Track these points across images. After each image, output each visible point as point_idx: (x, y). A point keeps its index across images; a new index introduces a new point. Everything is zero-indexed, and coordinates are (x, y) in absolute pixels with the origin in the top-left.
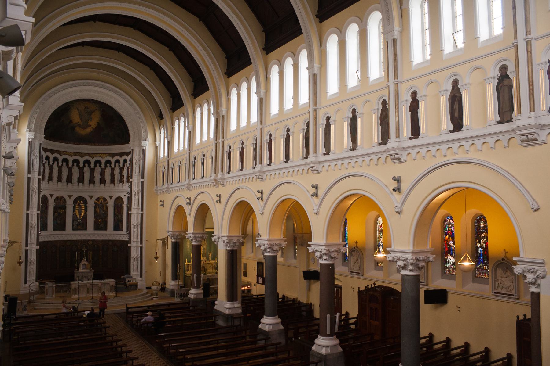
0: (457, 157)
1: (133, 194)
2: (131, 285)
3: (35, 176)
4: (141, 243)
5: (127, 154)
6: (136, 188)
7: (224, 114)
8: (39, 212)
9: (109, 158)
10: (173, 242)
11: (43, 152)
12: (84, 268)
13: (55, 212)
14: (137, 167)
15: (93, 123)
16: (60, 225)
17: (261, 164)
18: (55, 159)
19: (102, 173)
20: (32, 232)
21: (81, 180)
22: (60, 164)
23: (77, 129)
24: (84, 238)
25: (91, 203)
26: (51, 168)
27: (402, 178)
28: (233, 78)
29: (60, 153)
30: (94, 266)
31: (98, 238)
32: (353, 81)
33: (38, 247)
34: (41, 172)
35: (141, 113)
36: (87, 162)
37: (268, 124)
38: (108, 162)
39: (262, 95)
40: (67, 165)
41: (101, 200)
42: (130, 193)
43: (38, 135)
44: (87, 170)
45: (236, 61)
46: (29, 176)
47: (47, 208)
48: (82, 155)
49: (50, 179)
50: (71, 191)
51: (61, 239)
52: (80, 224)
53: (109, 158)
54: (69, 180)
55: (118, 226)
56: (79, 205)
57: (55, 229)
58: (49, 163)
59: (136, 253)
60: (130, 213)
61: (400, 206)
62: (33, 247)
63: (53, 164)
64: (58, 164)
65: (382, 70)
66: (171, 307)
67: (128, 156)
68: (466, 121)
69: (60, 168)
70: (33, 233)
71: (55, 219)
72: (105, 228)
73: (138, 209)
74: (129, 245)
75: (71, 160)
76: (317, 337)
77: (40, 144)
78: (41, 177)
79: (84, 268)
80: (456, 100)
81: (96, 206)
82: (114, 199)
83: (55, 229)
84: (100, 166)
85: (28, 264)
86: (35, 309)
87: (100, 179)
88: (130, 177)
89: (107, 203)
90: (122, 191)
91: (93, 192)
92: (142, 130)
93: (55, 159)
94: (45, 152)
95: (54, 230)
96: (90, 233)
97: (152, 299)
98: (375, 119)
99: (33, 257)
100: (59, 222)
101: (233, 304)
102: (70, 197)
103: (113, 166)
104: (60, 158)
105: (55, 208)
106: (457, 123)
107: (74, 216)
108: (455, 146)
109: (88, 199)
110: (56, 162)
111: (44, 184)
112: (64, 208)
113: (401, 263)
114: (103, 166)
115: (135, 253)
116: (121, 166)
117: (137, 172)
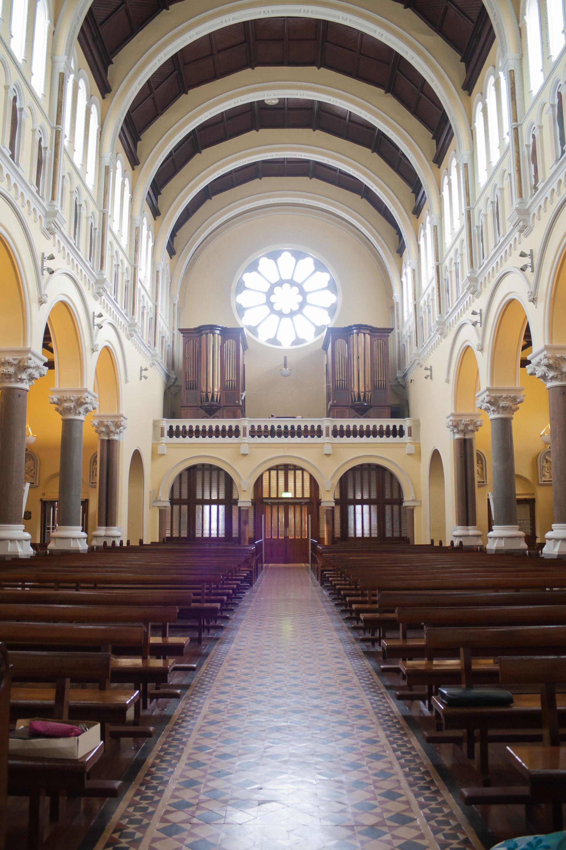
7: (398, 301)
17: (417, 346)
101: (468, 530)
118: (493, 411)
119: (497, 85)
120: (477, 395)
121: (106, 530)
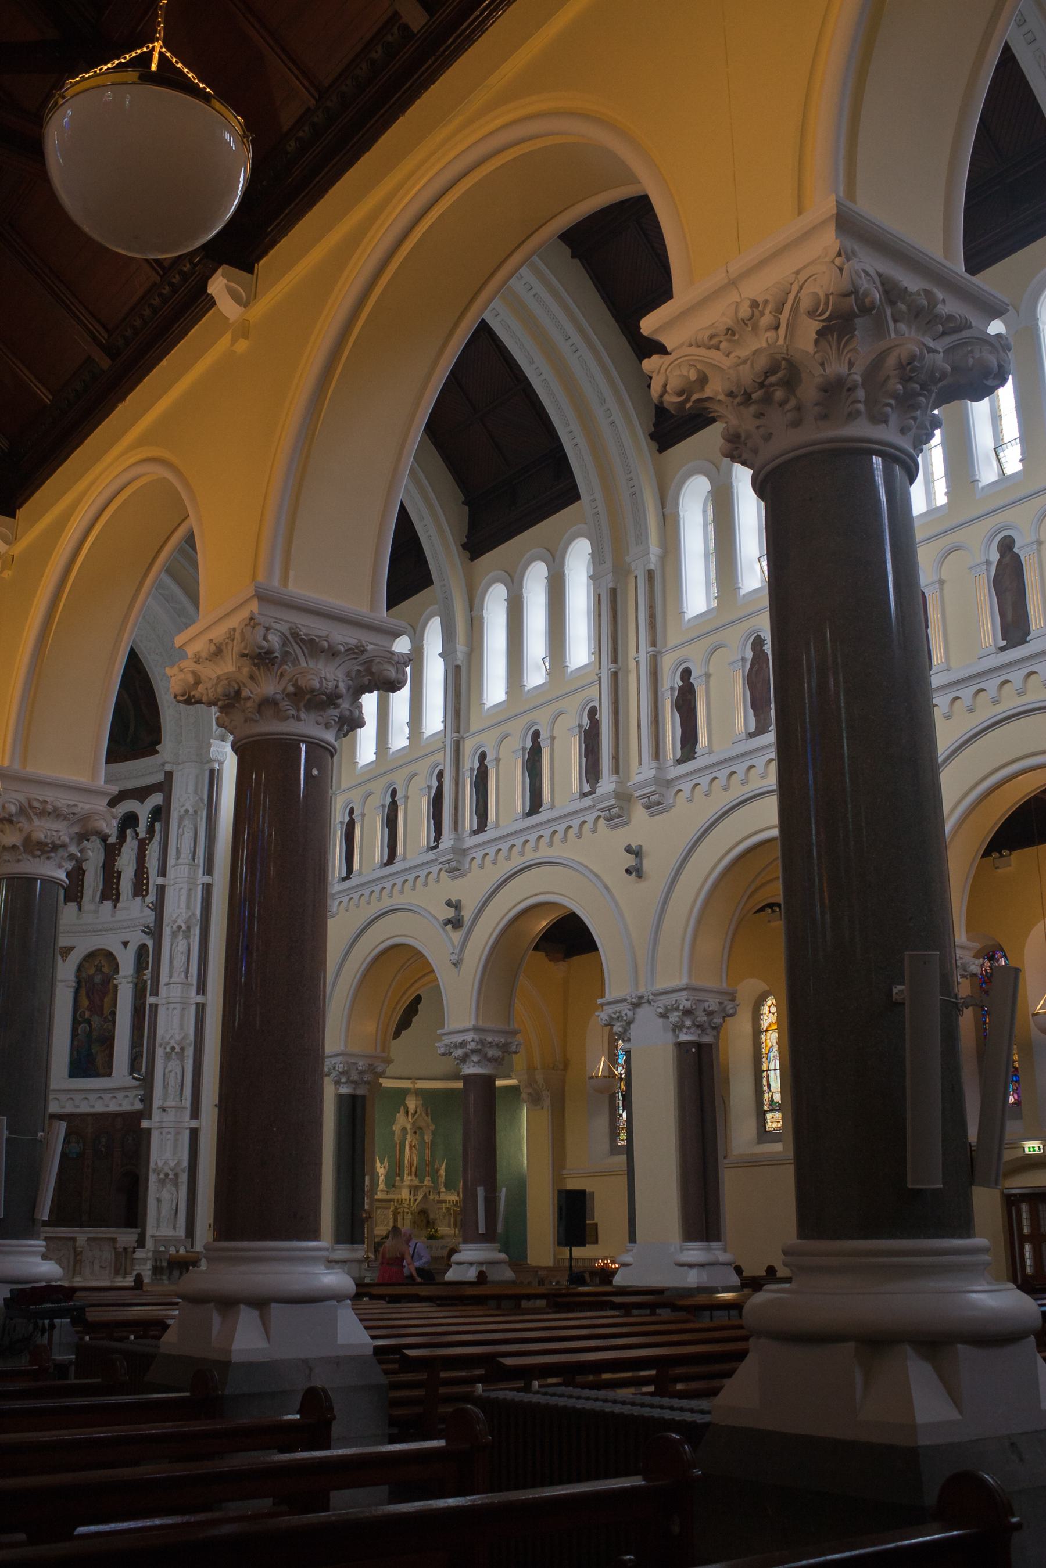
0: (1024, 700)
1: (167, 932)
10: (340, 1097)
14: (188, 836)
27: (644, 848)
28: (486, 559)
32: (535, 676)
37: (473, 728)
39: (460, 657)
42: (155, 931)
61: (457, 951)
65: (713, 597)
68: (1036, 619)
73: (186, 985)
74: (145, 1124)
98: (424, 807)
103: (142, 830)
108: (1017, 676)
113: (459, 1052)
115: (168, 1155)
116: (142, 835)
118: (479, 1062)
119: (722, 506)
120: (439, 1032)
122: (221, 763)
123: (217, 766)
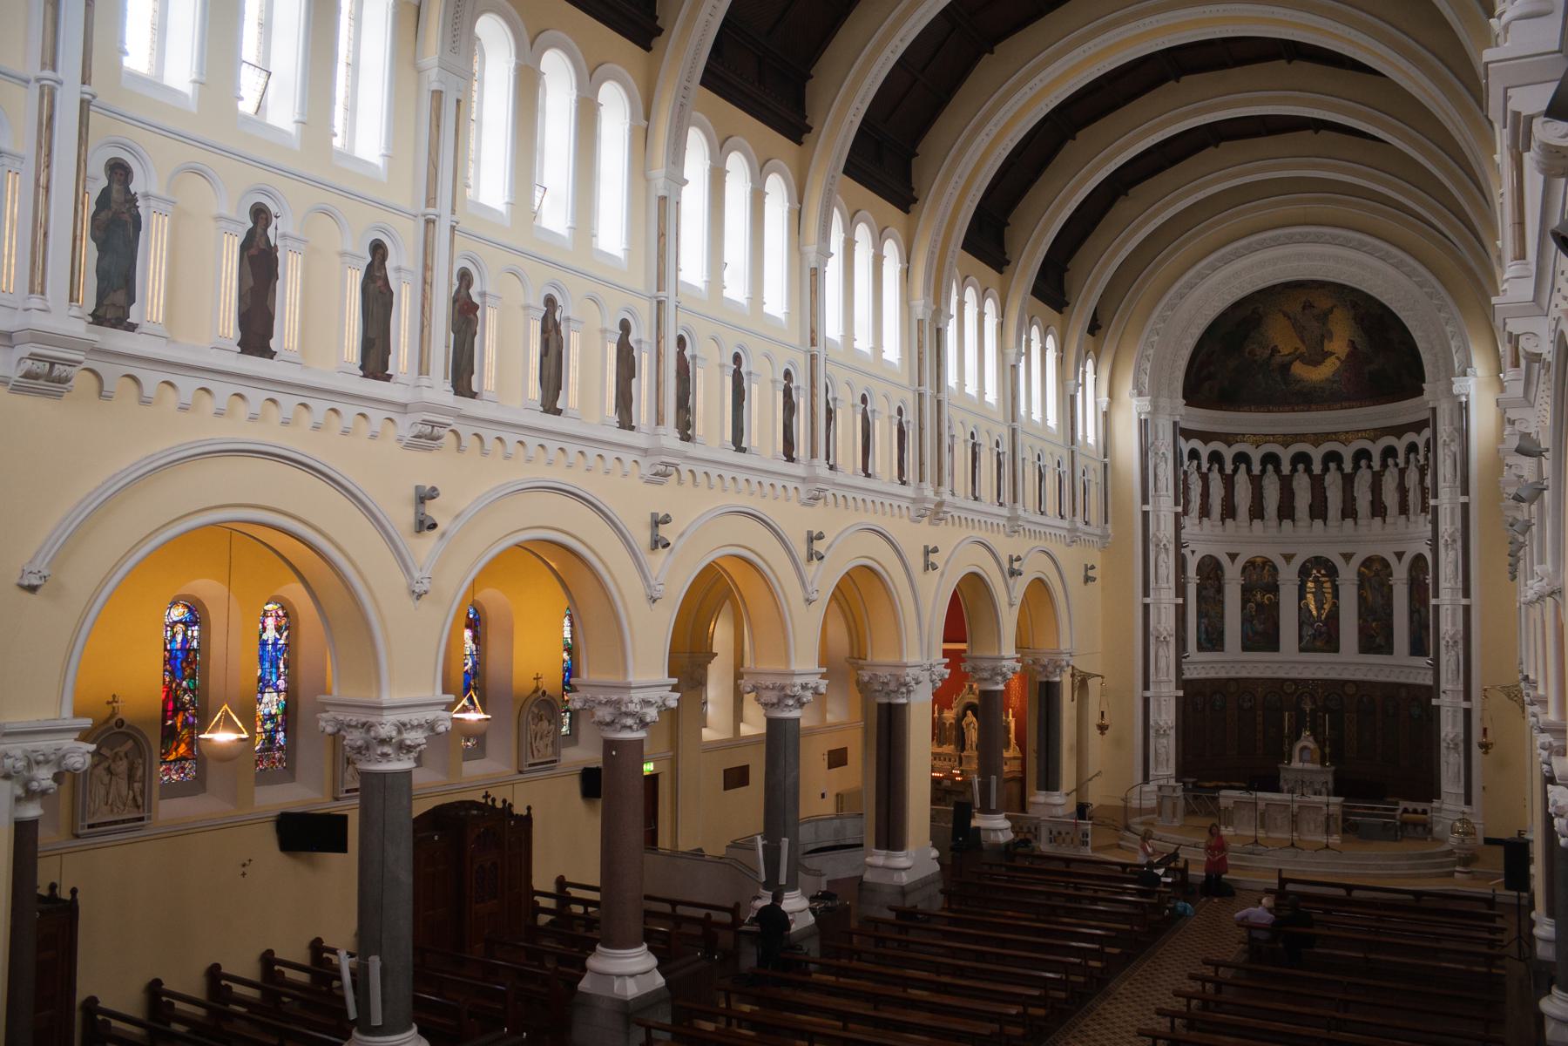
2: (1415, 824)
3: (1165, 506)
4: (1467, 697)
5: (1418, 427)
6: (1448, 526)
8: (1433, 602)
9: (1366, 444)
11: (1182, 441)
12: (1303, 759)
13: (1245, 602)
14: (1449, 462)
15: (1339, 346)
16: (1262, 635)
18: (1241, 458)
19: (1376, 487)
20: (1161, 652)
21: (1318, 510)
22: (1256, 469)
23: (1298, 369)
24: (1333, 675)
25: (1348, 576)
26: (1229, 482)
29: (1228, 439)
30: (1333, 752)
31: (1371, 677)
33: (1181, 693)
34: (1181, 492)
35: (1443, 292)
36: (1333, 457)
38: (1390, 452)
40: (1278, 470)
41: (1377, 566)
43: (1164, 402)
44: (1333, 482)
45: (887, 164)
46: (1146, 508)
47: (1220, 590)
48: (1317, 439)
49: (1229, 511)
50: (1288, 543)
51: (1268, 674)
52: (1322, 636)
53: (1366, 444)
54: (1286, 511)
55: (1419, 646)
56: (1316, 580)
57: (1246, 647)
58: (1221, 470)
59: (1454, 726)
60: (1180, 601)
62: (1166, 695)
63: (1235, 470)
64: (1249, 470)
66: (1074, 868)
67: (1419, 432)
69: (1256, 483)
70: (1165, 657)
71: (1246, 620)
72: (1387, 648)
74: (1434, 702)
75: (1286, 456)
76: (594, 949)
77: (1175, 424)
78: (1180, 509)
79: (1303, 759)
80: (259, 265)
81: (1363, 582)
82: (1407, 559)
83: (1246, 647)
84: (1340, 468)
85: (1152, 732)
86: (1119, 846)
87: (1372, 503)
88: (1428, 492)
89: (1391, 575)
90: (1413, 535)
91: (1347, 541)
92: (1453, 344)
93: (1241, 458)
94: (1187, 440)
95: (1245, 648)
96: (1349, 662)
97: (1451, 874)
99: (1166, 716)
100: (1260, 628)
102: (1288, 558)
103: (1401, 461)
104: (1228, 453)
105: (1247, 592)
106: (256, 332)
107: (1303, 611)
109: (1339, 563)
110: (1243, 467)
111: (1191, 524)
112: (1274, 588)
114: (1376, 465)
115: (1449, 728)
116: (1422, 462)
117: (1448, 476)
121: (887, 857)
122: (1467, 396)
123: (1464, 399)
